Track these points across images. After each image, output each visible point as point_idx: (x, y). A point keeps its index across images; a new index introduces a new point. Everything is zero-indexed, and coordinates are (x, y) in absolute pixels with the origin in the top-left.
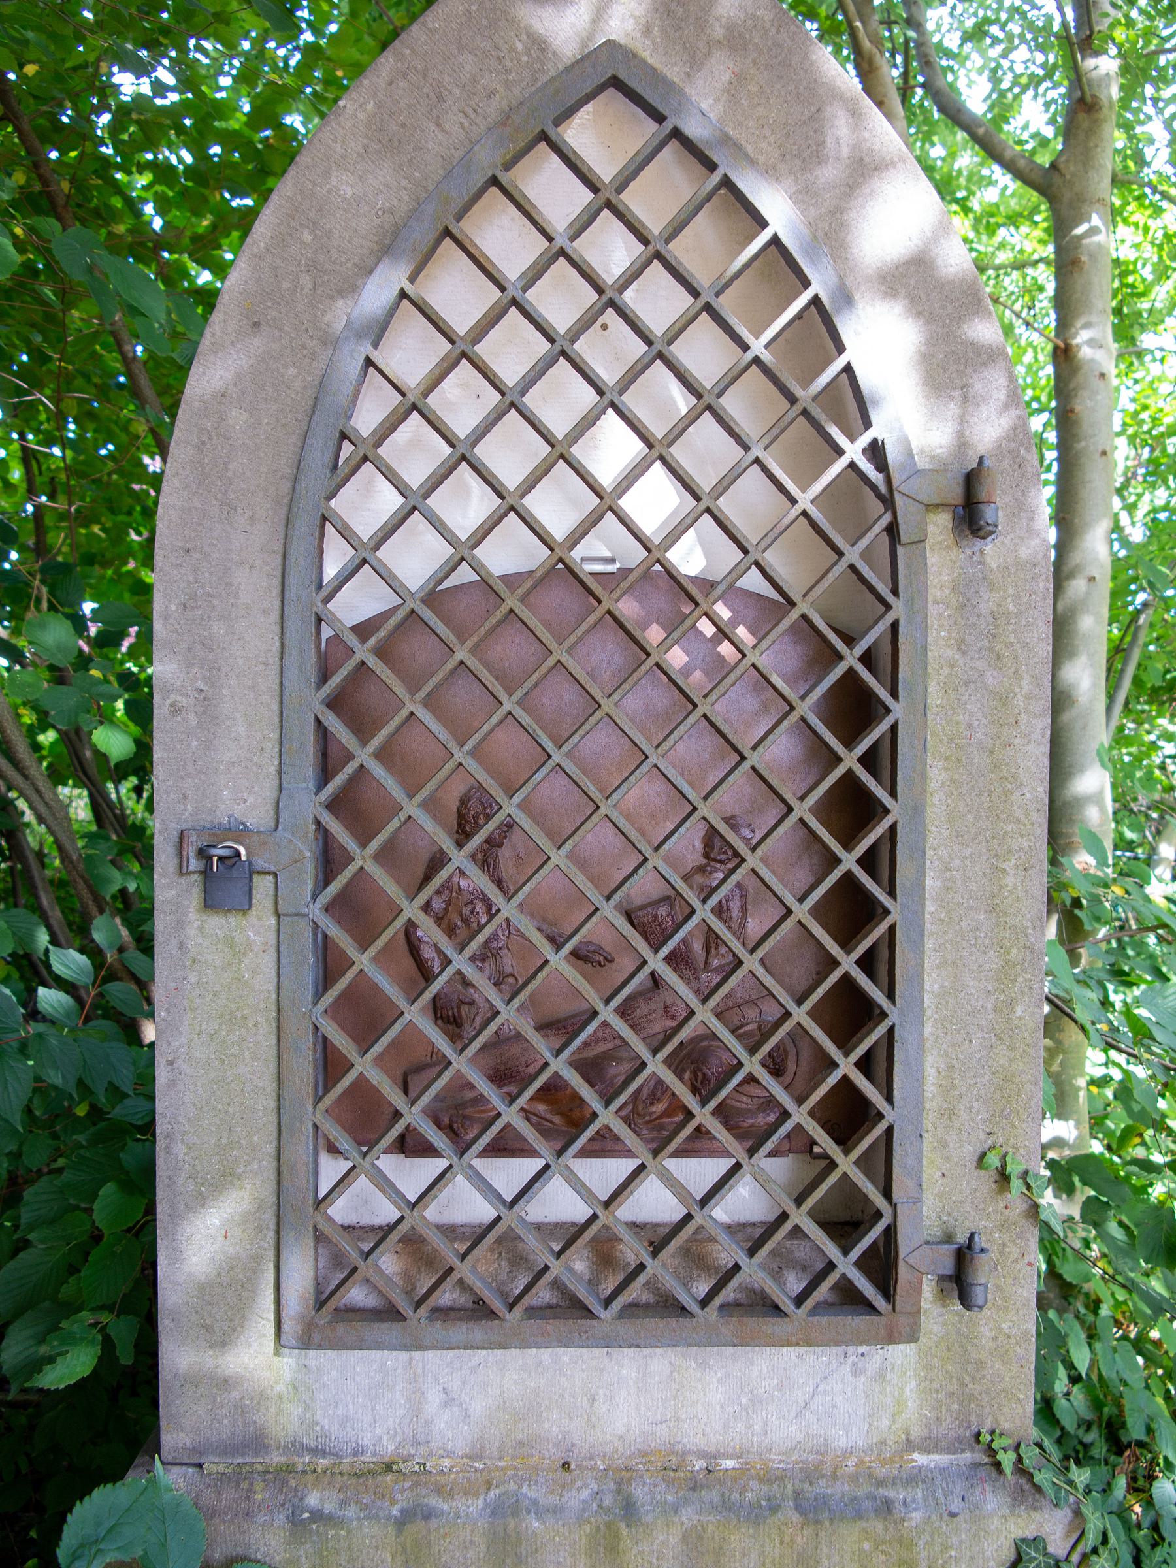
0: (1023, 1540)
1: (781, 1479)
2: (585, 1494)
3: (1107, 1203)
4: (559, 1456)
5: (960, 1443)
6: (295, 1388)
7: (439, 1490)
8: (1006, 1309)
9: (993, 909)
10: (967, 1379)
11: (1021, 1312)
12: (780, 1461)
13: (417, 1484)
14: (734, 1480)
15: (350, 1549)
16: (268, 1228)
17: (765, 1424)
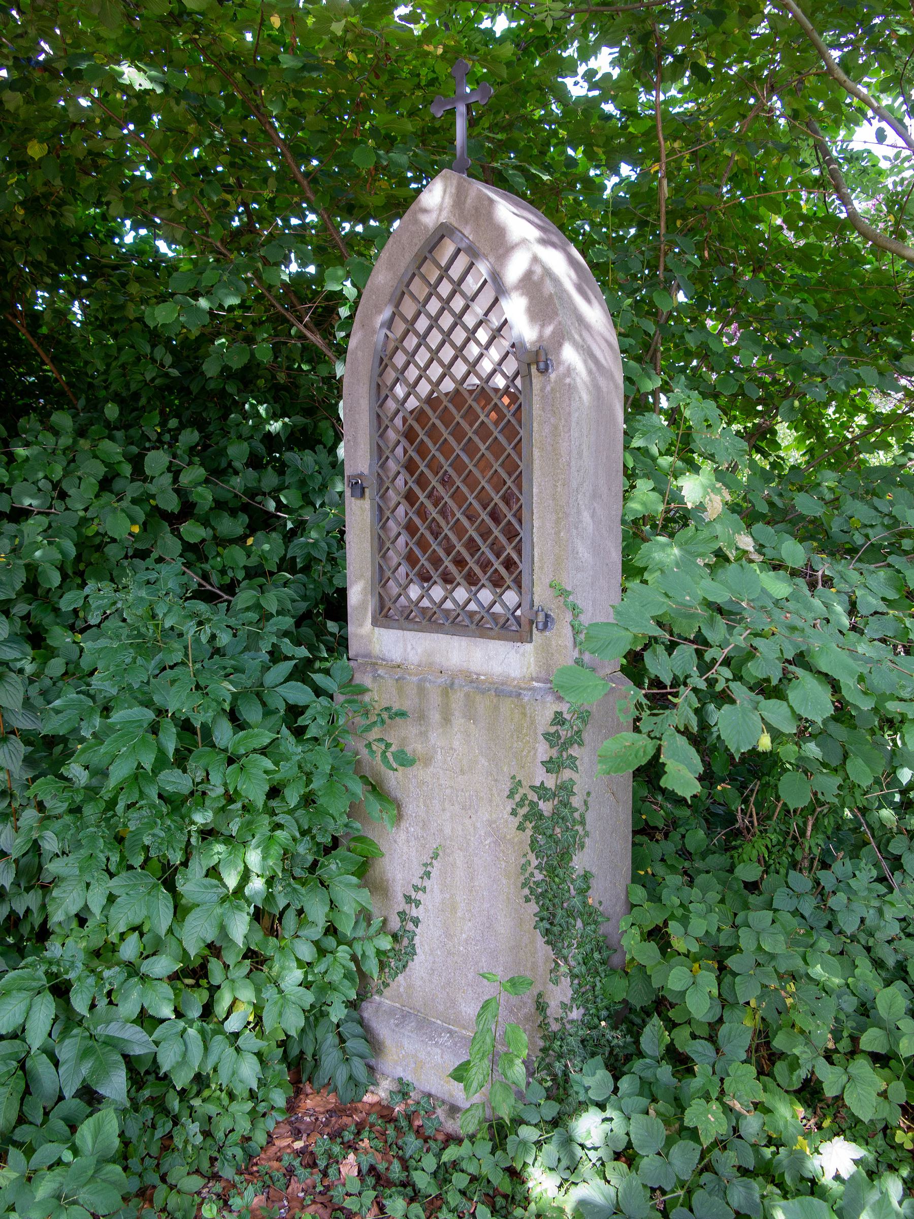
9: (554, 499)
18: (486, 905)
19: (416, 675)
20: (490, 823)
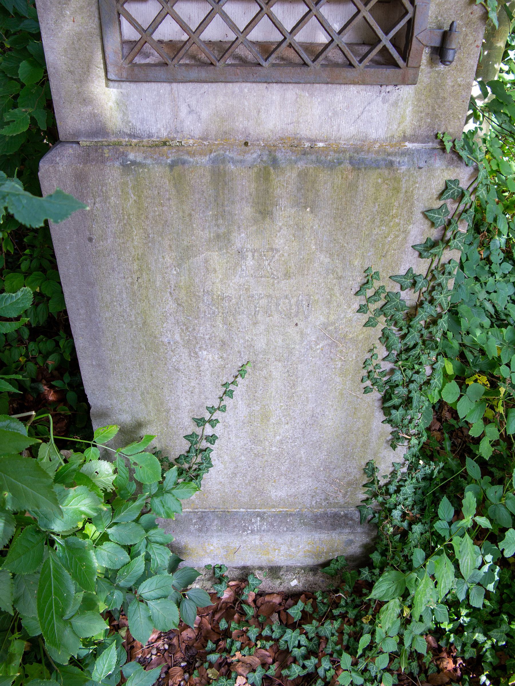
0: (449, 181)
1: (344, 152)
2: (255, 155)
3: (502, 103)
4: (242, 138)
5: (428, 138)
6: (118, 104)
7: (188, 153)
8: (461, 71)
10: (436, 106)
11: (468, 73)
12: (345, 144)
13: (178, 151)
14: (323, 151)
15: (150, 177)
16: (95, 16)
17: (339, 125)
18: (310, 406)
19: (202, 153)
20: (325, 326)
